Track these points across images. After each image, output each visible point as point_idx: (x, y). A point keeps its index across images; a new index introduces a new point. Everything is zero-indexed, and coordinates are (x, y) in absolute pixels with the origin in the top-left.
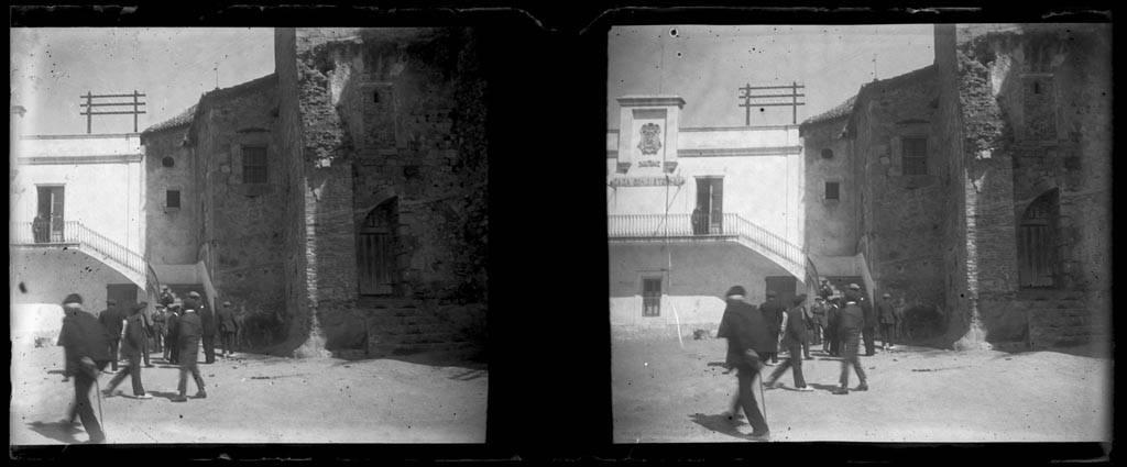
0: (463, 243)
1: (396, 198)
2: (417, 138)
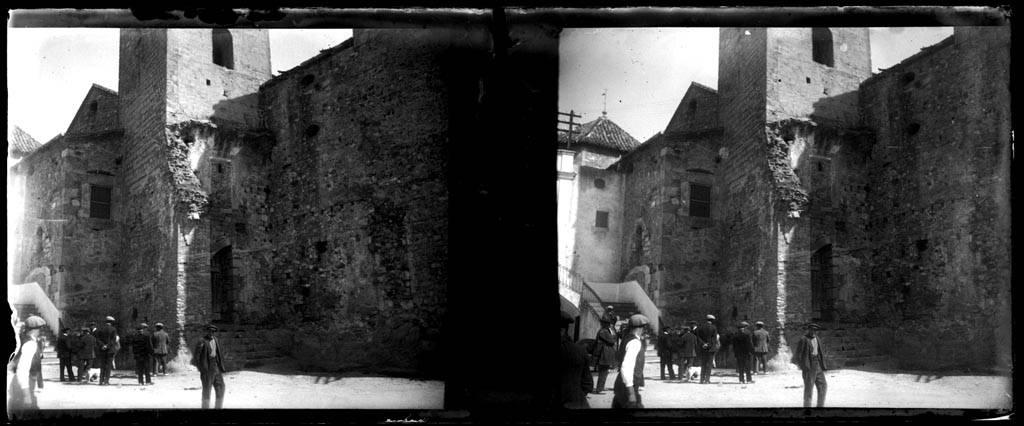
0: (871, 282)
1: (230, 247)
2: (245, 203)
